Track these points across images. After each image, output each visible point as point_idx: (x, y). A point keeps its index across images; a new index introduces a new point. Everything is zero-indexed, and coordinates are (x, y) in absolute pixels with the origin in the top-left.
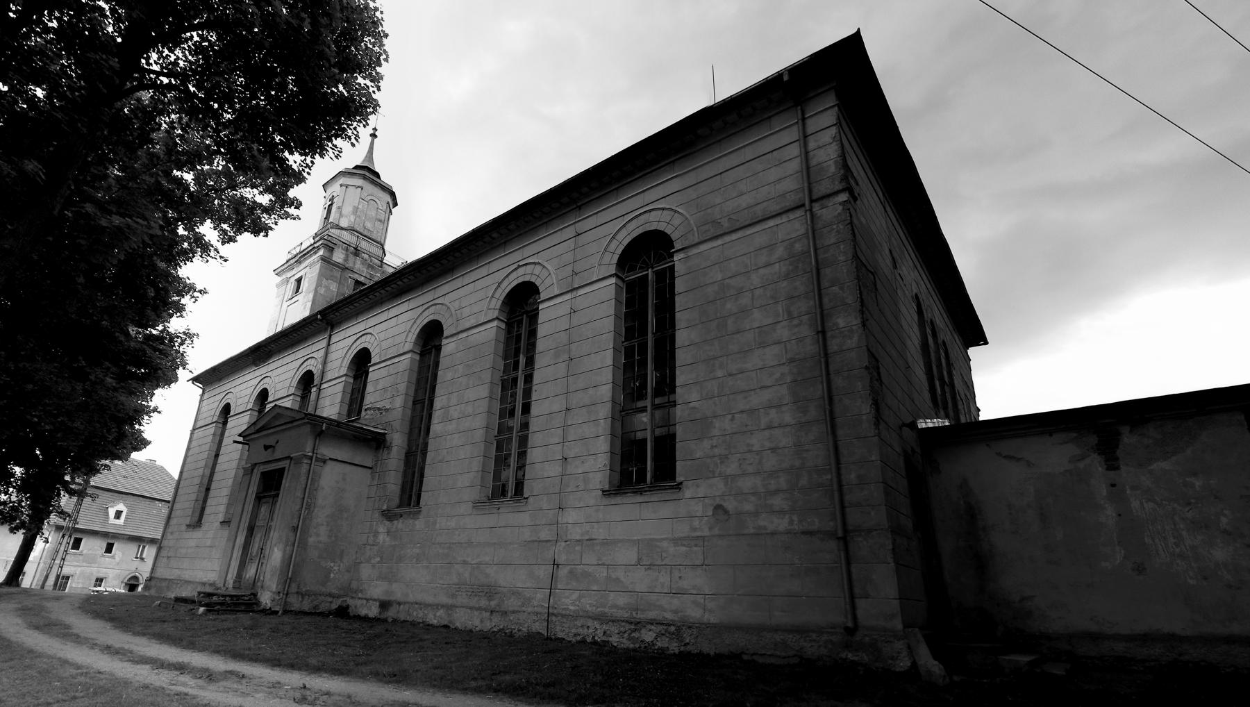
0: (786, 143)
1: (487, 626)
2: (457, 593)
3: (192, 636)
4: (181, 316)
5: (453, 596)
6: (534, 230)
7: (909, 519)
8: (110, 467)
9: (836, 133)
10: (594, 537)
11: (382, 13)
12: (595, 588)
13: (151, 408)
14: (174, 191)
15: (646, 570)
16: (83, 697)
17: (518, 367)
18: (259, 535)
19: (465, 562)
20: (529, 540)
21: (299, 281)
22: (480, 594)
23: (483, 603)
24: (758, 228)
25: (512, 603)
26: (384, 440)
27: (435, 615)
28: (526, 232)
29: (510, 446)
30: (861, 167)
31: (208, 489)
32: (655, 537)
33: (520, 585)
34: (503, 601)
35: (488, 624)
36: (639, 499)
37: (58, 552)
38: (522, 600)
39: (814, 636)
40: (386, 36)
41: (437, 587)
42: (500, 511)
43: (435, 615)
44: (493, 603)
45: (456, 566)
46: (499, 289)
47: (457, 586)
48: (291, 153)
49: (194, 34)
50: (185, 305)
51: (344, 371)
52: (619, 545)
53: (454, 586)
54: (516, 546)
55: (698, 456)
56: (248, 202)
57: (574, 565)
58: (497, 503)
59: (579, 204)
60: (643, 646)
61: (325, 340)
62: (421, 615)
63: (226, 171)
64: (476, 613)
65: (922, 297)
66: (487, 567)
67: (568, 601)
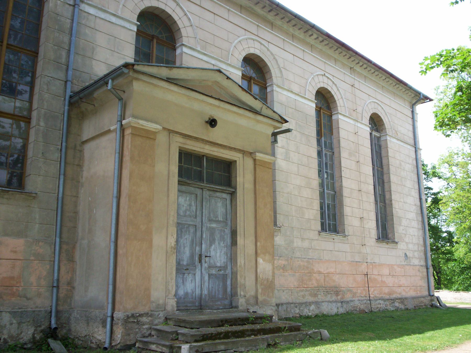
0: (318, 69)
1: (341, 311)
2: (318, 293)
3: (206, 198)
4: (436, 128)
5: (316, 295)
6: (307, 21)
7: (41, 244)
8: (407, 259)
9: (158, 129)
10: (375, 262)
11: (442, 52)
12: (378, 286)
13: (20, 19)
14: (138, 351)
15: (392, 277)
16: (465, 130)
17: (324, 144)
18: (166, 349)
19: (320, 273)
20: (351, 260)
21: (186, 239)
22: (332, 292)
23: (334, 298)
24: (110, 300)
25: (348, 297)
26: (71, 330)
27: (309, 310)
28: (119, 165)
29: (328, 196)
30: (227, 105)
31: (147, 137)
32: (215, 57)
33: (350, 286)
34: (344, 295)
35: (342, 310)
36: (387, 246)
37: (58, 287)
38: (352, 294)
39: (390, 300)
40: (421, 149)
41: (303, 290)
42: (334, 241)
43: (309, 310)
44: (339, 297)
45: (314, 275)
46: (183, 14)
47: (317, 289)
48: (20, 20)
49: (9, 23)
50: (420, 280)
51: (28, 160)
52: (30, 63)
53: (315, 289)
54: (346, 263)
55: (260, 260)
56: (224, 297)
57: (371, 275)
58: (334, 235)
59: (355, 78)
60: (12, 183)
61: (112, 136)
62: (297, 311)
63: (15, 73)
64: (334, 304)
65: (406, 93)
66: (333, 276)
67: (374, 293)
